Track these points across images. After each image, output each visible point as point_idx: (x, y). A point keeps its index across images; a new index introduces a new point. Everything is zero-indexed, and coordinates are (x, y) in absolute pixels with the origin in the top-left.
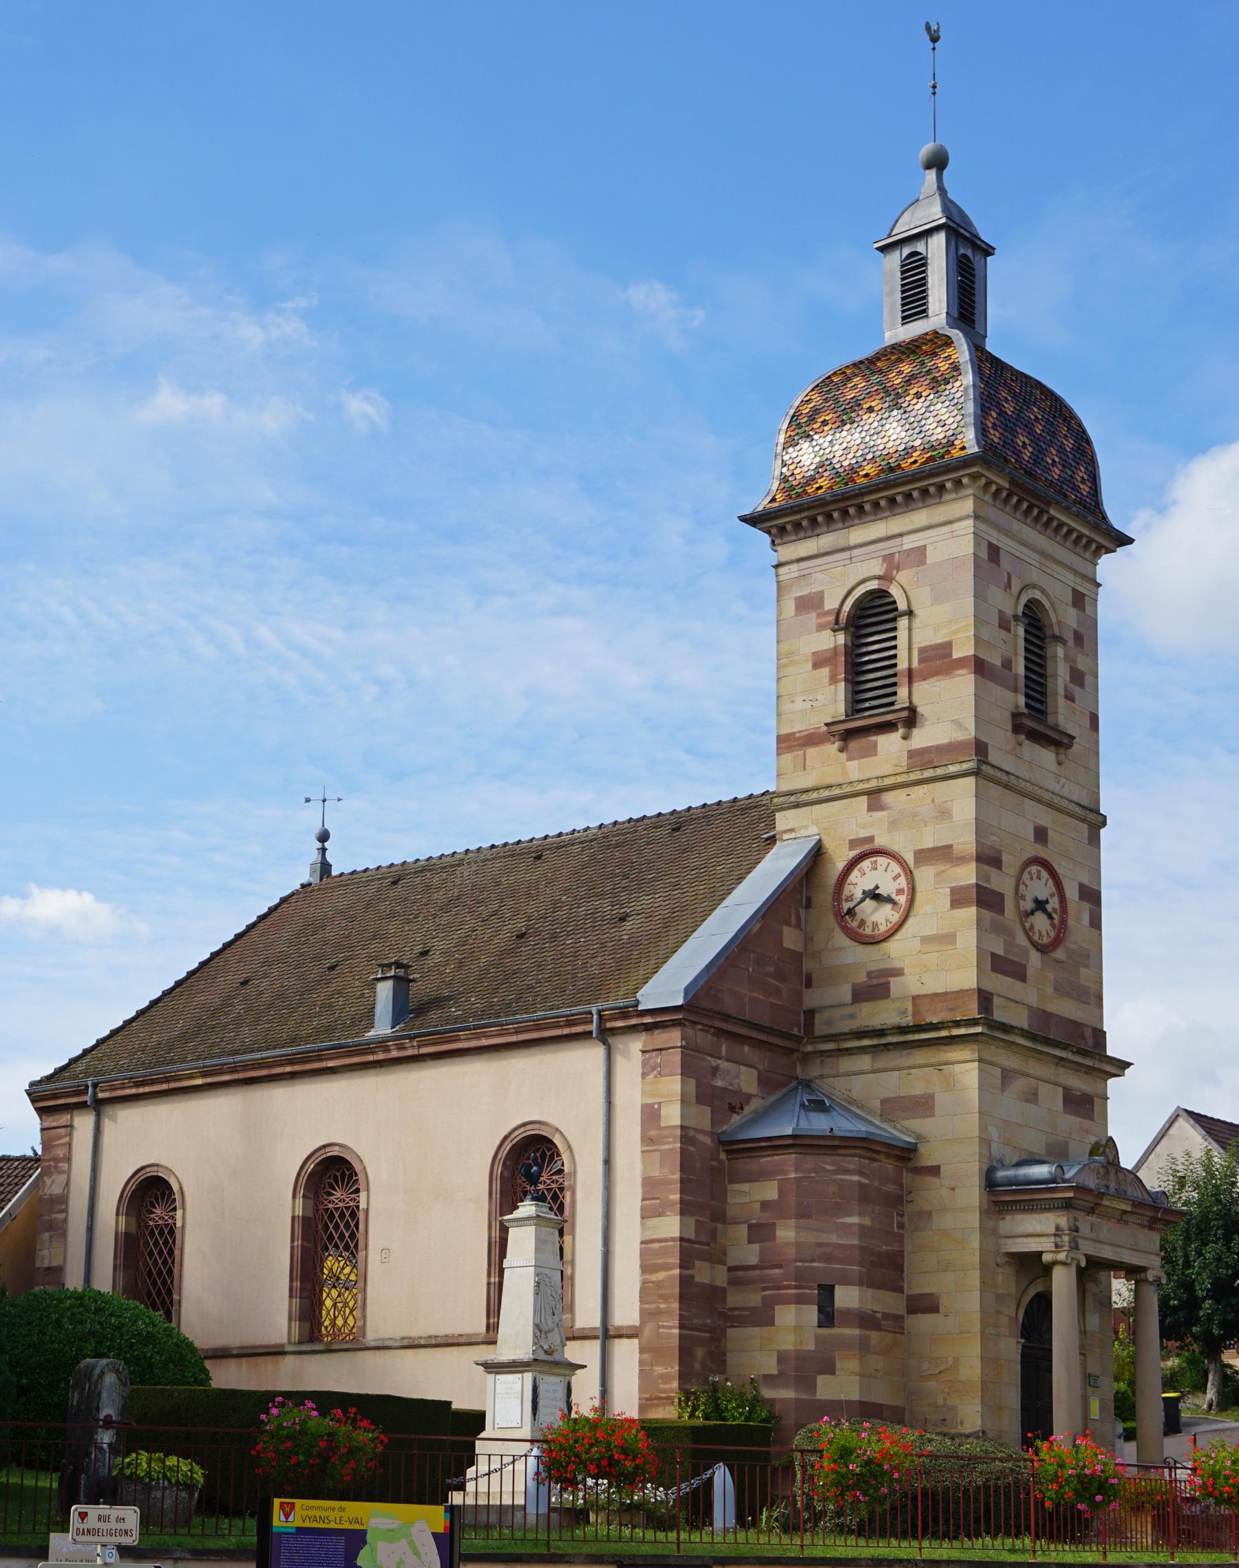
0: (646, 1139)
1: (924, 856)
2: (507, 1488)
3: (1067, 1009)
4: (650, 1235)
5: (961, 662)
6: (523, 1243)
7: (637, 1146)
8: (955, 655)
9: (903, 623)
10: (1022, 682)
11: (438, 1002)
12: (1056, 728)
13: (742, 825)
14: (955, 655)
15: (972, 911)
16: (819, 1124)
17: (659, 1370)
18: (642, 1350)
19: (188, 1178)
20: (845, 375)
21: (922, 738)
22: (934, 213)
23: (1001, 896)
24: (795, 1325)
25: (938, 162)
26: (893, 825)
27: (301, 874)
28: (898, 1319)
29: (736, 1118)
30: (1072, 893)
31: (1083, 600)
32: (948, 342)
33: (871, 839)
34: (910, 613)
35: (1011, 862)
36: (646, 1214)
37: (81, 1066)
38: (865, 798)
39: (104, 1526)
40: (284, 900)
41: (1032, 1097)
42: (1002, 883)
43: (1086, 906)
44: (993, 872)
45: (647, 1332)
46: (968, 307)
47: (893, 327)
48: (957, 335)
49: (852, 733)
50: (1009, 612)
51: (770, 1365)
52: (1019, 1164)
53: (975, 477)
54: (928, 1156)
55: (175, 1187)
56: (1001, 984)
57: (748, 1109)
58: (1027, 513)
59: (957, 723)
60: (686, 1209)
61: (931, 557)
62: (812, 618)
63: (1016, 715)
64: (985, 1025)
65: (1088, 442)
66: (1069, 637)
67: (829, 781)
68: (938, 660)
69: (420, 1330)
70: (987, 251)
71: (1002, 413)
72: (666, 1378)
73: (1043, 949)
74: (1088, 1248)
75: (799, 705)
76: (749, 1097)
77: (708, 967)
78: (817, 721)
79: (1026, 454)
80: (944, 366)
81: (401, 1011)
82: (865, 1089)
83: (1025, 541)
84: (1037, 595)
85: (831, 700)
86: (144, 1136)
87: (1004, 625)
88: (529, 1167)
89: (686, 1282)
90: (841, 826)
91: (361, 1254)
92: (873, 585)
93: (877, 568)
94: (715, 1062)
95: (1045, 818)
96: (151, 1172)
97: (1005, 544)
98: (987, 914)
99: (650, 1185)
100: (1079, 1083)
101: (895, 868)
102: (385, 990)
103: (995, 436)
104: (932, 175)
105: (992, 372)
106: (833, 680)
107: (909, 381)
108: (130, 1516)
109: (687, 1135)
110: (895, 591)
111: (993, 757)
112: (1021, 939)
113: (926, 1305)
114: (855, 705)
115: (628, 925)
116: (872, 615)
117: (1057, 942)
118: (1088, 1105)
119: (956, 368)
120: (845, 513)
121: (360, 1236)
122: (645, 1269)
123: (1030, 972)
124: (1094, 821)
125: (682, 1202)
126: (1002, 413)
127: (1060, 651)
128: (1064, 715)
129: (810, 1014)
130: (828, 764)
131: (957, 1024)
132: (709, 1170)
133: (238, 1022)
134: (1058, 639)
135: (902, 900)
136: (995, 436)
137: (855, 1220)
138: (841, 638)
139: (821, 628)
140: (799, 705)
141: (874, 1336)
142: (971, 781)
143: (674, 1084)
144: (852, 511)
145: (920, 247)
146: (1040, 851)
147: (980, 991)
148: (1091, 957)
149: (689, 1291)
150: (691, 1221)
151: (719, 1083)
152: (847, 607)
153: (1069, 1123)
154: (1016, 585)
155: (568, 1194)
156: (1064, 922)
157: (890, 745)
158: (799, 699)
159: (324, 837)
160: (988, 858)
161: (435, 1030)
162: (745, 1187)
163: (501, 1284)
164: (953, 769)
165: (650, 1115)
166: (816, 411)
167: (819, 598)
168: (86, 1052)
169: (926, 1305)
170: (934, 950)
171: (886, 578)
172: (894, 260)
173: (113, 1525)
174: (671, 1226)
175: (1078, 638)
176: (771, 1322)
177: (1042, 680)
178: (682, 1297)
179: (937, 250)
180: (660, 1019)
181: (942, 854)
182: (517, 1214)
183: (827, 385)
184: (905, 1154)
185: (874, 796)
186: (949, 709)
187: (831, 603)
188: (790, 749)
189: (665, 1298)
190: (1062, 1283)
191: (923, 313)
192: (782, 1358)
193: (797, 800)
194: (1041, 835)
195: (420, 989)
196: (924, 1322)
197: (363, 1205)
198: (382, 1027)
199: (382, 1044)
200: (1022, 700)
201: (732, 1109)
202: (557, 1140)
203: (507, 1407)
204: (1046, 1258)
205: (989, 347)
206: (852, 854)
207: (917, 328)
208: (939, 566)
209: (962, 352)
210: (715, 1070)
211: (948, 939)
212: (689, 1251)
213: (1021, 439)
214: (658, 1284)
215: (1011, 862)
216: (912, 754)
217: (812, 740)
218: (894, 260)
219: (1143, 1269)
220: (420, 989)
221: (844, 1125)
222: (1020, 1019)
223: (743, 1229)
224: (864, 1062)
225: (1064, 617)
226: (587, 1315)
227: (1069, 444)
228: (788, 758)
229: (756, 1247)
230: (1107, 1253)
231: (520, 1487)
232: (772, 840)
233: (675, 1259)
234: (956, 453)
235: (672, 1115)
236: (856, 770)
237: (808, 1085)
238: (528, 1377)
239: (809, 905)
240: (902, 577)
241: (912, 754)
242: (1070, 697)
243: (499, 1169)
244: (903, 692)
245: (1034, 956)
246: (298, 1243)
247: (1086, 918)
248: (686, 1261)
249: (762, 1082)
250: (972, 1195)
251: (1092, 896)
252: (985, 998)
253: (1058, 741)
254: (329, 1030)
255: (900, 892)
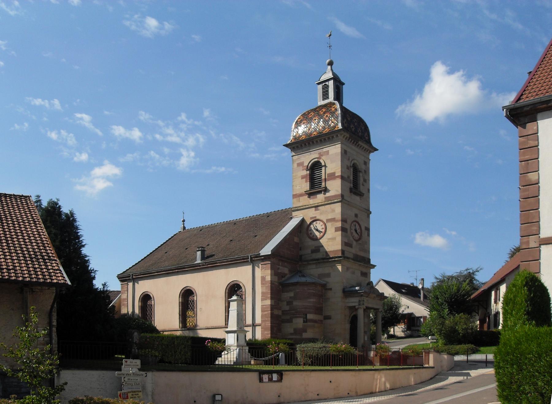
0: (262, 284)
1: (328, 220)
2: (232, 357)
3: (362, 254)
4: (263, 304)
5: (338, 177)
6: (234, 306)
7: (260, 285)
8: (336, 175)
9: (323, 168)
10: (352, 182)
11: (212, 256)
12: (360, 191)
13: (285, 215)
14: (336, 175)
15: (340, 233)
16: (303, 280)
17: (266, 332)
18: (262, 328)
19: (153, 293)
20: (309, 112)
21: (328, 194)
22: (329, 75)
23: (347, 229)
24: (299, 322)
25: (331, 64)
26: (321, 214)
27: (179, 229)
28: (321, 321)
29: (283, 279)
30: (363, 228)
31: (366, 163)
32: (334, 104)
33: (315, 217)
34: (325, 166)
35: (349, 221)
36: (262, 300)
37: (129, 271)
38: (314, 208)
39: (132, 364)
40: (175, 235)
41: (353, 273)
42: (347, 226)
43: (366, 232)
44: (345, 224)
45: (263, 325)
46: (338, 96)
47: (320, 101)
48: (336, 102)
49: (311, 194)
50: (349, 165)
51: (292, 331)
52: (351, 287)
53: (341, 135)
54: (329, 286)
55: (152, 296)
56: (347, 249)
57: (286, 277)
58: (353, 143)
59: (337, 191)
60: (272, 298)
61: (330, 153)
62: (301, 168)
63: (351, 189)
64: (344, 256)
65: (368, 127)
66: (363, 171)
67: (305, 204)
68: (332, 176)
69: (209, 325)
70: (343, 84)
71: (347, 120)
72: (267, 334)
73: (357, 241)
74: (366, 304)
75: (298, 188)
76: (286, 274)
77: (277, 246)
78: (303, 191)
79: (353, 130)
80: (333, 109)
81: (203, 258)
82: (314, 272)
83: (353, 150)
84: (356, 162)
85: (306, 186)
86: (144, 286)
87: (348, 168)
88: (234, 289)
89: (272, 314)
90: (309, 215)
91: (195, 310)
92: (316, 160)
93: (317, 156)
94: (278, 267)
95: (357, 212)
96: (146, 293)
97: (348, 150)
98: (344, 233)
99: (263, 294)
100: (364, 270)
101: (322, 223)
102: (199, 253)
103: (346, 125)
104: (329, 67)
105: (345, 112)
106: (306, 181)
107: (324, 113)
108: (138, 362)
109: (272, 282)
110: (321, 161)
111: (345, 198)
112: (351, 239)
113: (328, 318)
114: (312, 186)
115: (257, 237)
116: (315, 167)
117: (360, 239)
118: (366, 275)
119: (336, 110)
120: (309, 144)
121: (195, 306)
122: (262, 311)
123: (353, 246)
124: (368, 213)
125: (271, 297)
126: (347, 120)
127: (361, 175)
128: (362, 189)
129: (301, 256)
130: (305, 201)
131: (336, 257)
132: (278, 290)
133: (165, 261)
134: (360, 171)
135: (323, 230)
136: (346, 125)
137: (312, 300)
138: (308, 172)
139: (303, 170)
140: (298, 188)
141: (316, 325)
142: (340, 204)
143: (269, 272)
144: (311, 143)
145: (327, 83)
146: (356, 219)
147: (342, 250)
148: (367, 243)
149: (273, 316)
150: (273, 301)
151: (279, 271)
152: (310, 165)
153: (362, 279)
154: (350, 160)
155: (244, 296)
156: (361, 235)
157: (320, 198)
158: (298, 186)
159: (184, 221)
160: (344, 220)
161: (210, 263)
162: (286, 294)
163: (228, 316)
164: (335, 201)
165: (263, 278)
166: (301, 121)
167: (303, 163)
168: (130, 268)
169: (328, 318)
170: (332, 242)
171: (319, 158)
172: (320, 86)
173: (134, 364)
174: (268, 302)
175: (365, 172)
176: (292, 322)
177: (356, 181)
178: (271, 317)
179: (331, 84)
180: (266, 258)
181: (333, 220)
182: (232, 299)
183: (304, 115)
184: (324, 286)
185: (316, 207)
186: (335, 187)
187: (306, 164)
188: (296, 197)
189: (267, 317)
190: (361, 313)
191: (328, 98)
192: (295, 330)
193: (297, 209)
194: (356, 216)
195: (207, 253)
196: (328, 321)
197: (195, 299)
198: (199, 261)
199: (198, 265)
200: (352, 185)
201: (283, 277)
202: (241, 284)
203: (231, 340)
204: (357, 307)
205: (344, 105)
206: (311, 220)
207: (326, 101)
208: (332, 157)
209: (338, 106)
210: (279, 268)
211: (333, 239)
212: (273, 307)
213: (352, 126)
214: (265, 315)
215: (349, 221)
216: (325, 198)
217: (301, 195)
218: (320, 86)
219: (378, 309)
220: (207, 253)
221: (309, 280)
222: (351, 256)
223: (285, 303)
224: (314, 266)
225: (362, 167)
226: (249, 321)
227: (363, 128)
228: (295, 199)
229: (288, 306)
230: (370, 306)
231: (235, 357)
232: (291, 218)
233: (269, 309)
234: (336, 129)
235: (268, 278)
236: (312, 201)
237: (301, 272)
238: (236, 334)
239: (300, 232)
240: (323, 158)
241: (325, 198)
242: (363, 185)
243: (227, 291)
244: (323, 184)
245: (354, 243)
246: (181, 307)
247: (366, 235)
248: (272, 309)
249: (290, 271)
250: (340, 294)
251: (368, 229)
252: (343, 252)
253: (361, 195)
254: (186, 262)
255: (322, 229)
